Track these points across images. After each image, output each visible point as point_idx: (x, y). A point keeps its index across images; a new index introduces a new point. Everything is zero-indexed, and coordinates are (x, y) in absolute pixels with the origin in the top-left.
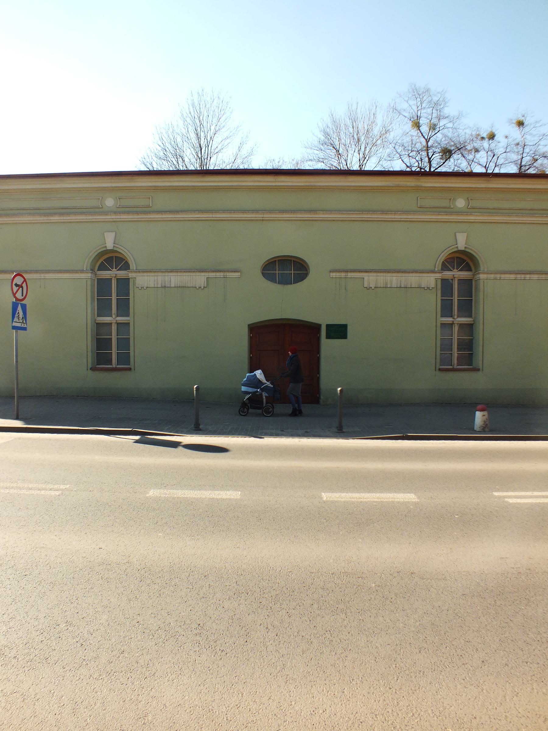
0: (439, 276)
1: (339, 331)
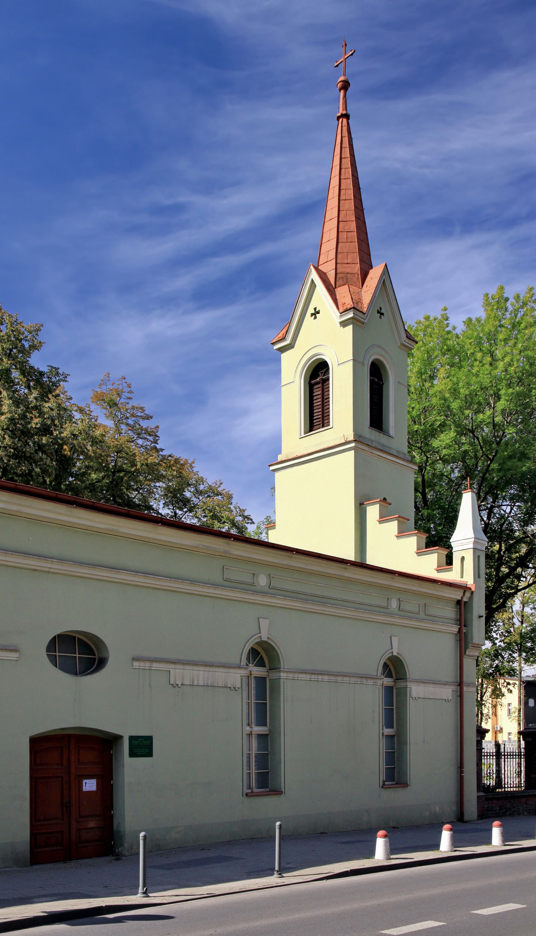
0: (244, 672)
1: (142, 747)
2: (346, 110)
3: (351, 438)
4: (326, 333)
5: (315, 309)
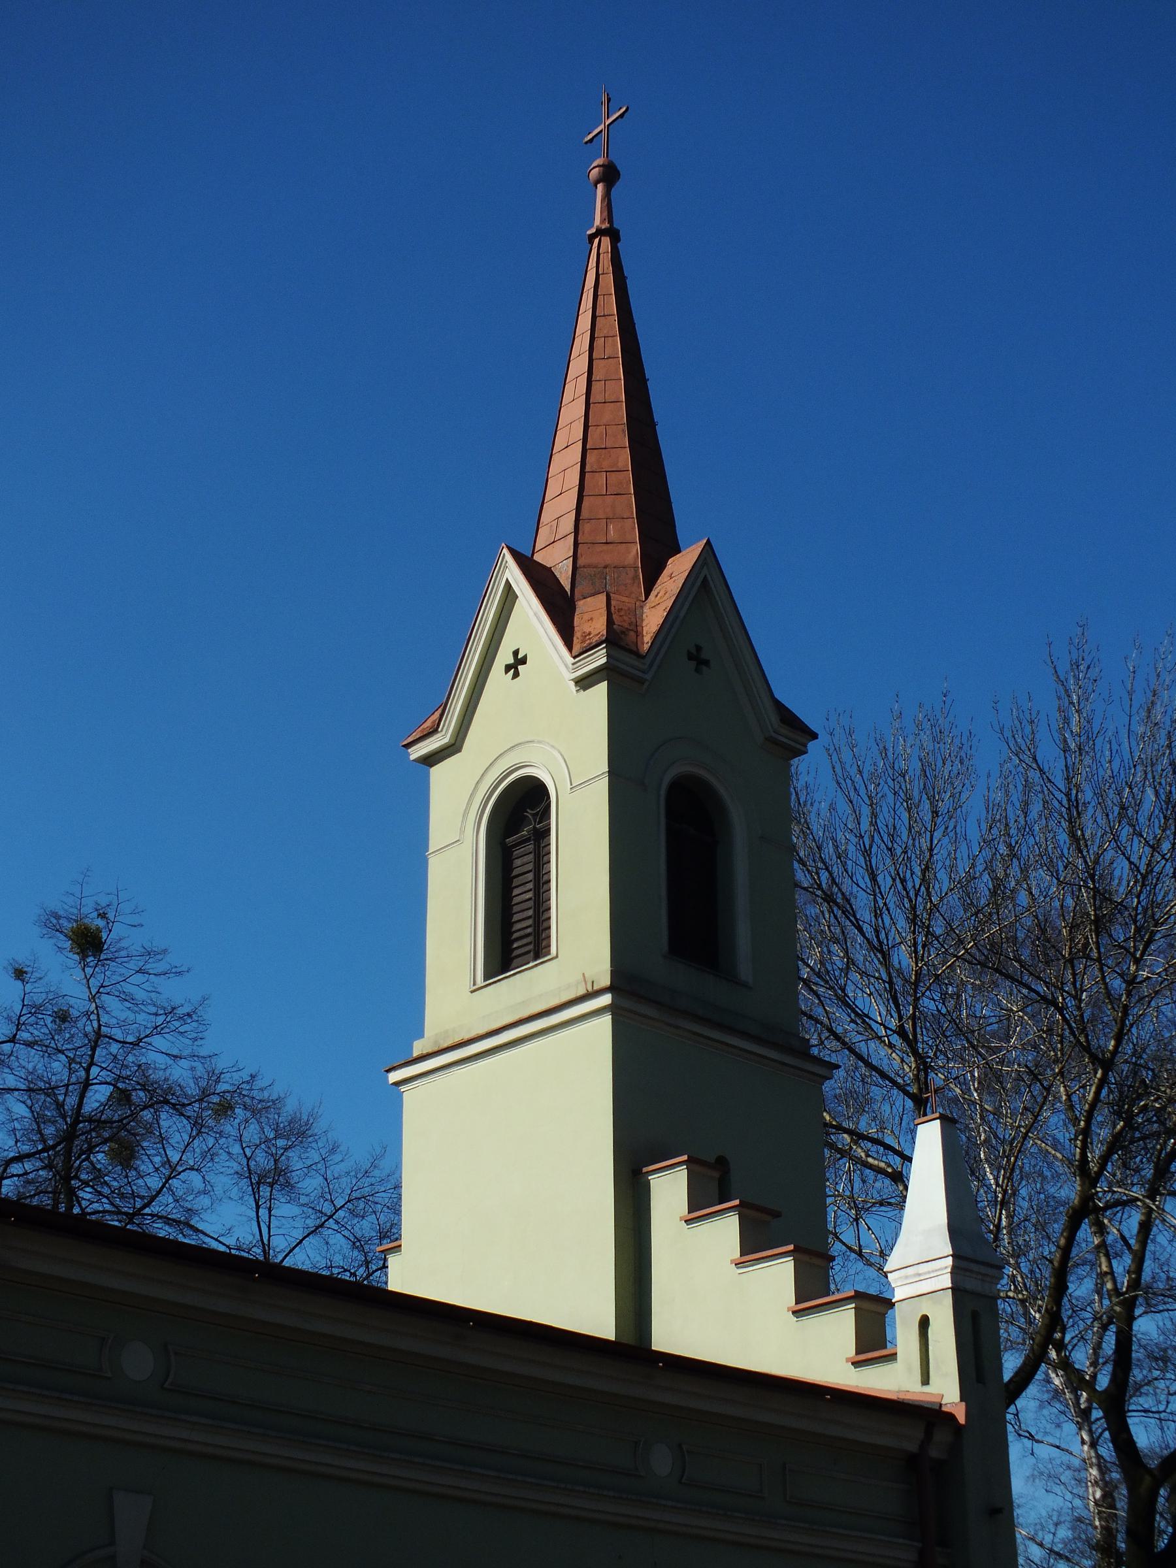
2: (611, 221)
3: (606, 981)
4: (543, 716)
5: (516, 653)
